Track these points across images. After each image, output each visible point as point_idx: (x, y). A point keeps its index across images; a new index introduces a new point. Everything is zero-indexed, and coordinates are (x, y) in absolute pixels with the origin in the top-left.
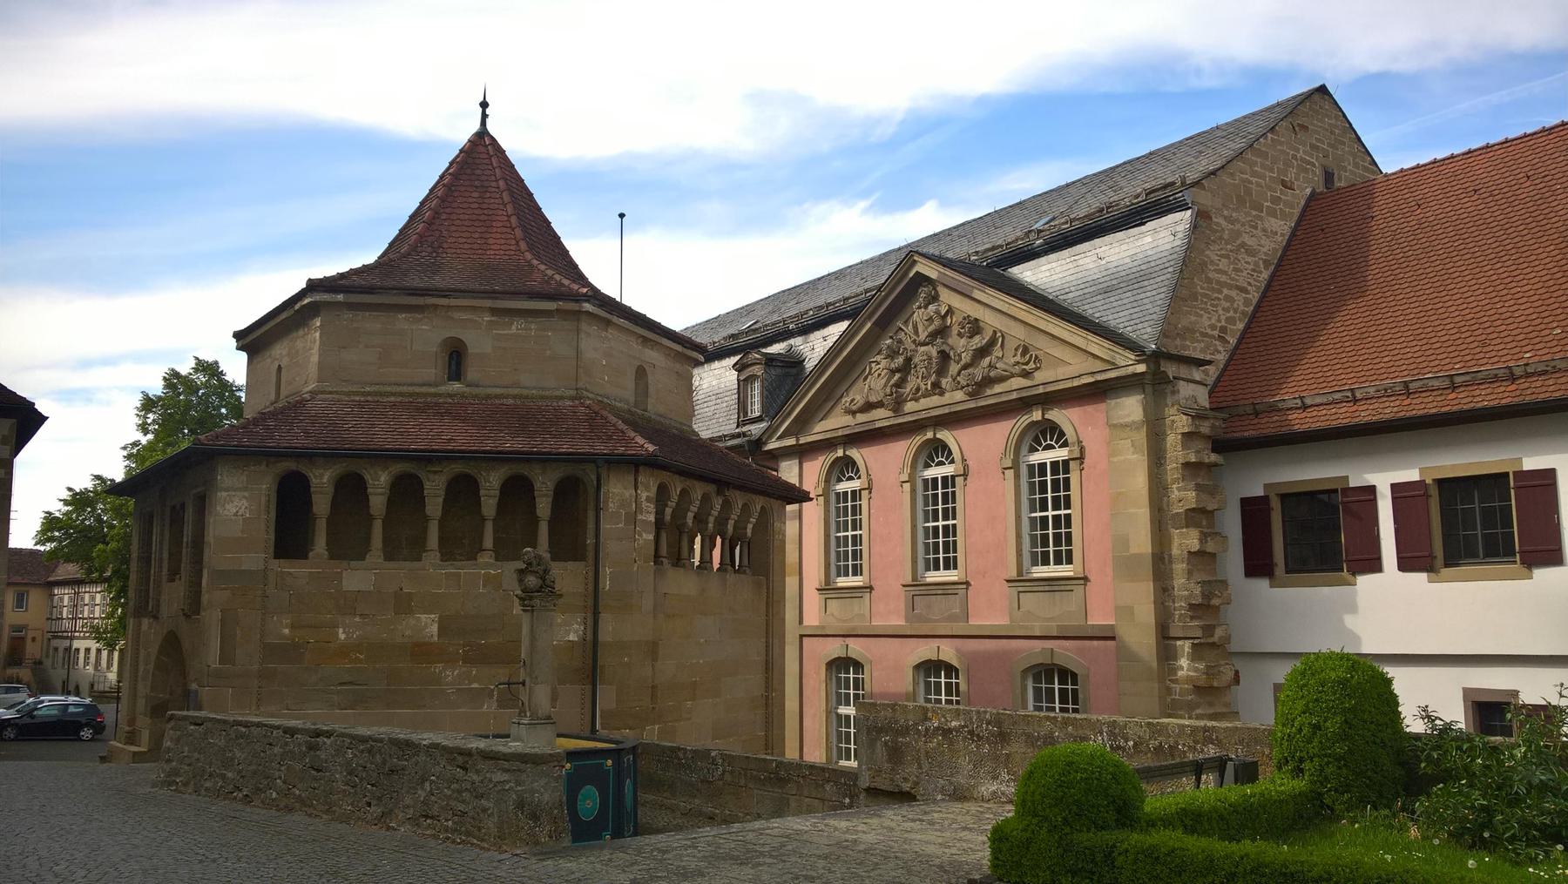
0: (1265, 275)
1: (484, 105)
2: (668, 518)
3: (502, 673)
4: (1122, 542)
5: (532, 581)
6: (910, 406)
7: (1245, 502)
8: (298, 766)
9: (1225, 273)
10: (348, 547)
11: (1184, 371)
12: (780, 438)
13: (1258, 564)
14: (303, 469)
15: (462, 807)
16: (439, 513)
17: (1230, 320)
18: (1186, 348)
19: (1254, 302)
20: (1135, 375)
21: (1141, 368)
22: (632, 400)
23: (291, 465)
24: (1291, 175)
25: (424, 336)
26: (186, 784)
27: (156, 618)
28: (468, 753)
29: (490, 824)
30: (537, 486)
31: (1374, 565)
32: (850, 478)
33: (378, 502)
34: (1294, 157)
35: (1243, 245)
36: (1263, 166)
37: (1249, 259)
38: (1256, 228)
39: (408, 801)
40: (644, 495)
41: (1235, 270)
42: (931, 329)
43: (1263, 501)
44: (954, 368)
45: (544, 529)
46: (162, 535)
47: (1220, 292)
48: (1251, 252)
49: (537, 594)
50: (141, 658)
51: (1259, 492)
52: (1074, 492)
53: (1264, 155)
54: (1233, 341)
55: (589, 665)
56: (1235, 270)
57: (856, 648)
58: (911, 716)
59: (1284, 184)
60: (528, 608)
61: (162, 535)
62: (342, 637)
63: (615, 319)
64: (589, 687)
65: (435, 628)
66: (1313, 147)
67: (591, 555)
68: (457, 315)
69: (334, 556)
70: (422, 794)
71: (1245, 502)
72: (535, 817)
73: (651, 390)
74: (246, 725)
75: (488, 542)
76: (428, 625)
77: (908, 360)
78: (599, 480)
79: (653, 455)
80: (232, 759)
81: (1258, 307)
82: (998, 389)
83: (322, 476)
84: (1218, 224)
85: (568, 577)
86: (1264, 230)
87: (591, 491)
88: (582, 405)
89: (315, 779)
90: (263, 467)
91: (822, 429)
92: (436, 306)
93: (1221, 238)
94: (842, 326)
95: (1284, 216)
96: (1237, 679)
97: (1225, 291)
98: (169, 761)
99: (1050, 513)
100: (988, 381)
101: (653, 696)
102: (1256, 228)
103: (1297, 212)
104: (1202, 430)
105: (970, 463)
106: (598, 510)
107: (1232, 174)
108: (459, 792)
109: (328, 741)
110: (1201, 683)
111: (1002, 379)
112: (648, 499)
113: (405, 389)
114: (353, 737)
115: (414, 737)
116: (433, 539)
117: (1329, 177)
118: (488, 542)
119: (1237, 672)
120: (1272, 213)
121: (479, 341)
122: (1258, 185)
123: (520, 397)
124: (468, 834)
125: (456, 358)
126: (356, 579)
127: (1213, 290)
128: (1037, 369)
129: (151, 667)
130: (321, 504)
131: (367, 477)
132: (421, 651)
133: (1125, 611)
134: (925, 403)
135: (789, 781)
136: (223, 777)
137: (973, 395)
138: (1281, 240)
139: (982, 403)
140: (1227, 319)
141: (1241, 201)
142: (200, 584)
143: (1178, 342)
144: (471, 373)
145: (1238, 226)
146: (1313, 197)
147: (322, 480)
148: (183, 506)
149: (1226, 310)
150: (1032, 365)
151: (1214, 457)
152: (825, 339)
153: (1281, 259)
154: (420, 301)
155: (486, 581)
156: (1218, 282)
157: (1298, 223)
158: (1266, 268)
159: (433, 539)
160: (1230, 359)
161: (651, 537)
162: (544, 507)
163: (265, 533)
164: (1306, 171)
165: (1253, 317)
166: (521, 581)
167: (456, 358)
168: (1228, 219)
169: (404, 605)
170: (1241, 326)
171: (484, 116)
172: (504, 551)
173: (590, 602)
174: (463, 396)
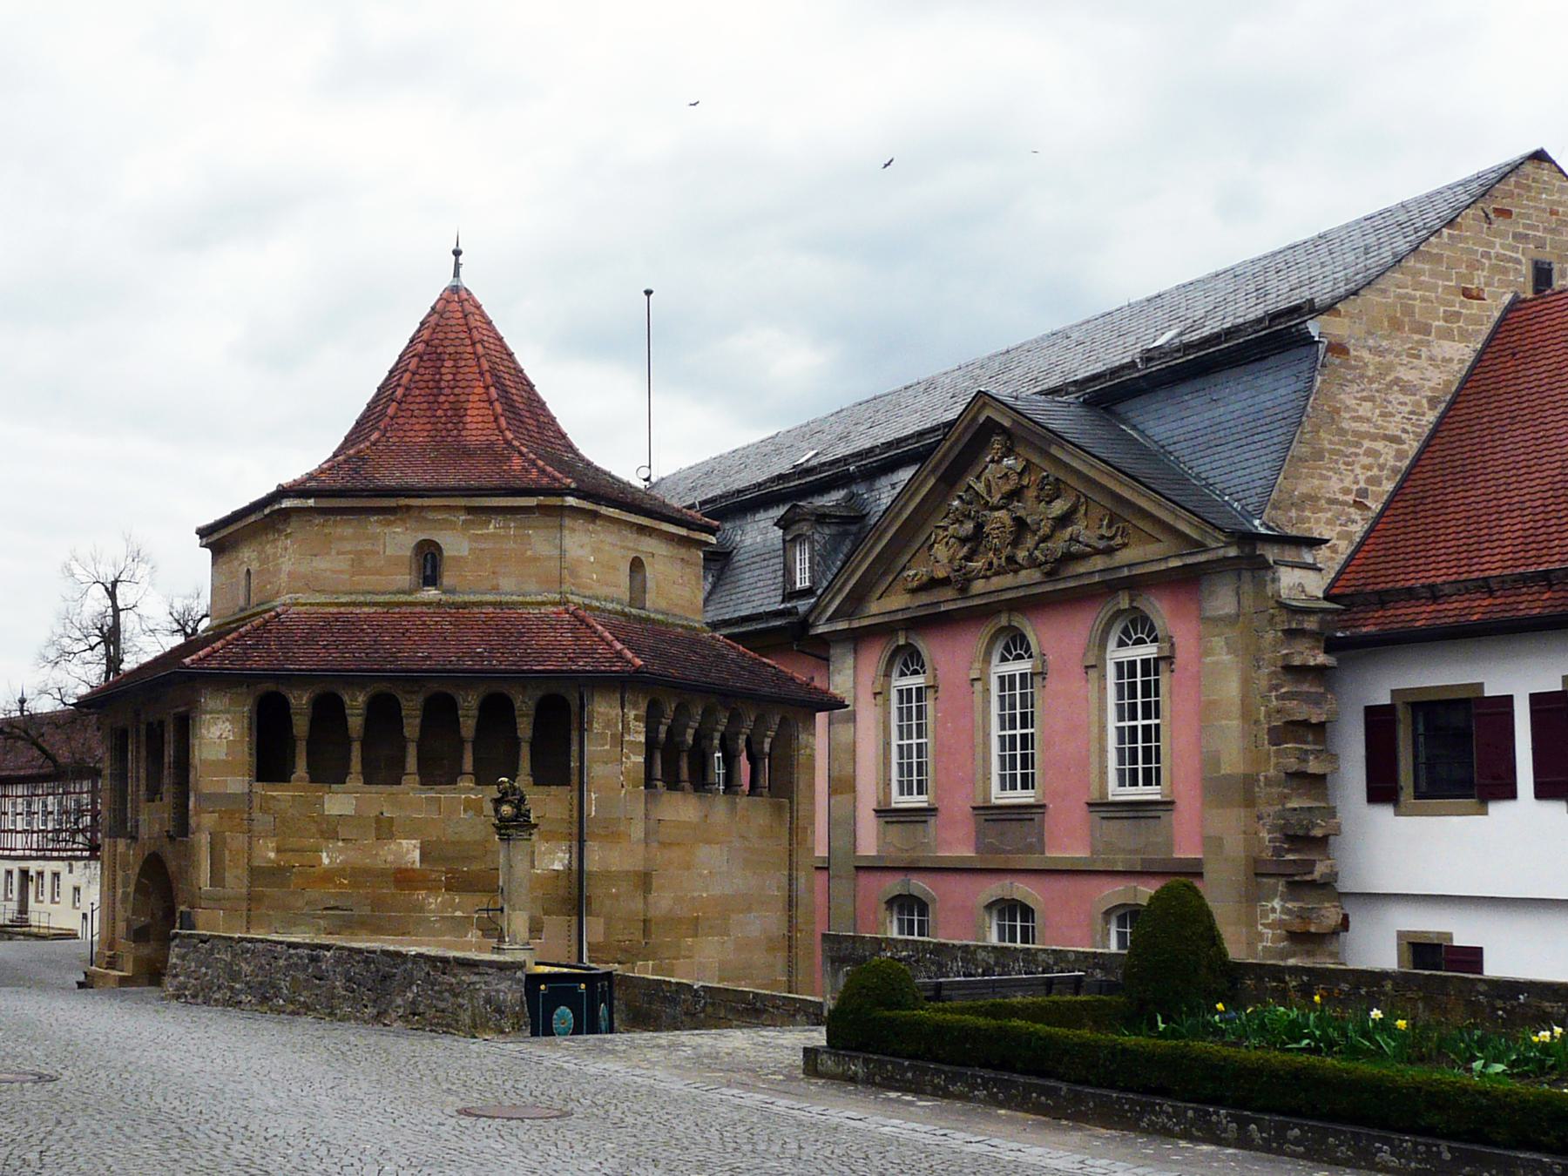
0: (1431, 417)
1: (457, 253)
2: (662, 736)
3: (483, 900)
4: (1213, 760)
5: (506, 809)
6: (978, 586)
7: (1371, 712)
8: (302, 977)
9: (1368, 420)
10: (328, 772)
11: (1290, 554)
12: (830, 620)
13: (1382, 790)
14: (283, 690)
15: (442, 1005)
16: (417, 735)
17: (1372, 481)
18: (1302, 520)
19: (1412, 454)
20: (1226, 558)
21: (1232, 552)
22: (626, 597)
23: (270, 686)
24: (1479, 279)
25: (400, 540)
26: (194, 996)
27: (134, 838)
28: (445, 960)
29: (465, 1017)
30: (517, 704)
31: (1510, 793)
32: (916, 672)
33: (355, 722)
34: (1486, 255)
35: (1397, 381)
36: (1433, 274)
37: (1407, 399)
38: (1418, 357)
39: (399, 1001)
40: (632, 714)
41: (1383, 415)
42: (1006, 488)
43: (1388, 710)
44: (1030, 541)
45: (525, 751)
46: (138, 752)
47: (1358, 445)
48: (1407, 388)
49: (515, 825)
50: (119, 880)
51: (1385, 699)
52: (1164, 699)
53: (1438, 259)
54: (1376, 506)
55: (574, 896)
56: (1383, 415)
57: (920, 885)
58: (867, 947)
59: (1467, 293)
60: (506, 838)
61: (138, 752)
62: (326, 861)
63: (604, 510)
64: (575, 919)
65: (417, 854)
66: (1516, 236)
67: (575, 779)
68: (431, 515)
69: (315, 778)
70: (410, 995)
71: (1371, 712)
72: (499, 1010)
73: (650, 584)
74: (251, 941)
75: (468, 764)
76: (409, 852)
77: (979, 527)
78: (582, 699)
79: (638, 670)
80: (239, 972)
81: (1417, 459)
82: (1082, 568)
83: (301, 698)
84: (1356, 358)
85: (546, 804)
86: (1431, 358)
87: (575, 708)
88: (567, 611)
89: (319, 987)
90: (244, 689)
91: (879, 607)
92: (408, 508)
93: (1362, 376)
94: (905, 475)
95: (1465, 336)
96: (1345, 924)
97: (1367, 444)
98: (176, 976)
99: (1140, 723)
100: (1069, 558)
101: (646, 932)
102: (1418, 357)
103: (1486, 329)
104: (1307, 626)
105: (1050, 658)
106: (582, 731)
107: (1384, 291)
108: (441, 992)
109: (328, 954)
110: (1297, 927)
111: (1083, 557)
112: (637, 718)
113: (381, 599)
114: (351, 949)
115: (404, 950)
116: (412, 763)
117: (1542, 275)
118: (468, 764)
119: (1346, 918)
120: (1446, 335)
121: (454, 543)
122: (1424, 299)
123: (499, 604)
124: (448, 1025)
125: (429, 562)
126: (339, 803)
127: (1349, 444)
128: (1125, 545)
129: (131, 889)
130: (301, 726)
131: (346, 698)
132: (404, 878)
133: (1213, 843)
134: (997, 582)
135: (765, 1011)
136: (232, 989)
137: (1051, 575)
138: (1457, 370)
139: (1061, 586)
140: (1369, 480)
141: (1396, 325)
142: (187, 806)
143: (1293, 513)
144: (447, 580)
145: (1390, 357)
146: (1515, 305)
147: (300, 701)
148: (161, 723)
149: (1368, 468)
150: (1119, 540)
151: (1321, 659)
152: (893, 486)
153: (1458, 393)
154: (392, 502)
155: (464, 807)
156: (1355, 433)
157: (1488, 343)
158: (1432, 407)
159: (412, 763)
160: (1371, 530)
161: (641, 759)
162: (525, 729)
163: (245, 755)
164: (1505, 271)
165: (1408, 475)
166: (497, 811)
167: (429, 562)
168: (1379, 352)
169: (385, 829)
170: (1389, 486)
171: (457, 266)
172: (482, 779)
173: (575, 830)
174: (439, 604)
